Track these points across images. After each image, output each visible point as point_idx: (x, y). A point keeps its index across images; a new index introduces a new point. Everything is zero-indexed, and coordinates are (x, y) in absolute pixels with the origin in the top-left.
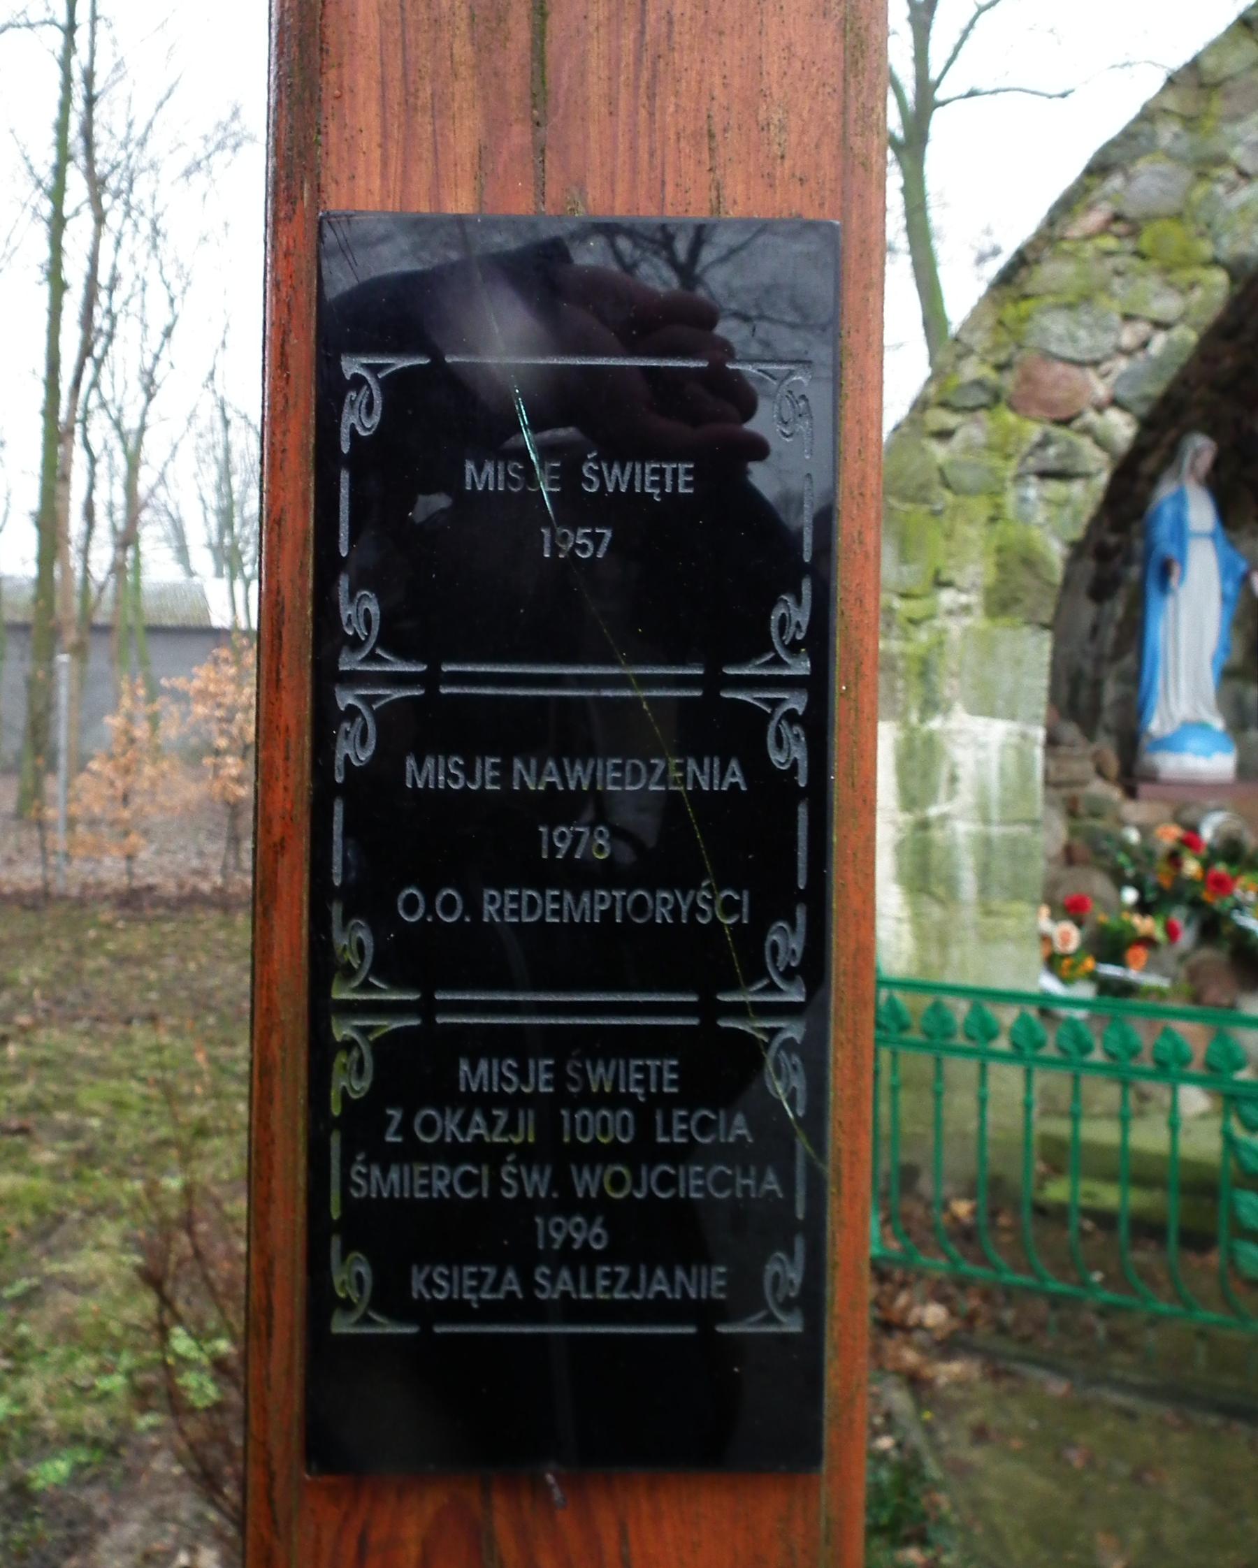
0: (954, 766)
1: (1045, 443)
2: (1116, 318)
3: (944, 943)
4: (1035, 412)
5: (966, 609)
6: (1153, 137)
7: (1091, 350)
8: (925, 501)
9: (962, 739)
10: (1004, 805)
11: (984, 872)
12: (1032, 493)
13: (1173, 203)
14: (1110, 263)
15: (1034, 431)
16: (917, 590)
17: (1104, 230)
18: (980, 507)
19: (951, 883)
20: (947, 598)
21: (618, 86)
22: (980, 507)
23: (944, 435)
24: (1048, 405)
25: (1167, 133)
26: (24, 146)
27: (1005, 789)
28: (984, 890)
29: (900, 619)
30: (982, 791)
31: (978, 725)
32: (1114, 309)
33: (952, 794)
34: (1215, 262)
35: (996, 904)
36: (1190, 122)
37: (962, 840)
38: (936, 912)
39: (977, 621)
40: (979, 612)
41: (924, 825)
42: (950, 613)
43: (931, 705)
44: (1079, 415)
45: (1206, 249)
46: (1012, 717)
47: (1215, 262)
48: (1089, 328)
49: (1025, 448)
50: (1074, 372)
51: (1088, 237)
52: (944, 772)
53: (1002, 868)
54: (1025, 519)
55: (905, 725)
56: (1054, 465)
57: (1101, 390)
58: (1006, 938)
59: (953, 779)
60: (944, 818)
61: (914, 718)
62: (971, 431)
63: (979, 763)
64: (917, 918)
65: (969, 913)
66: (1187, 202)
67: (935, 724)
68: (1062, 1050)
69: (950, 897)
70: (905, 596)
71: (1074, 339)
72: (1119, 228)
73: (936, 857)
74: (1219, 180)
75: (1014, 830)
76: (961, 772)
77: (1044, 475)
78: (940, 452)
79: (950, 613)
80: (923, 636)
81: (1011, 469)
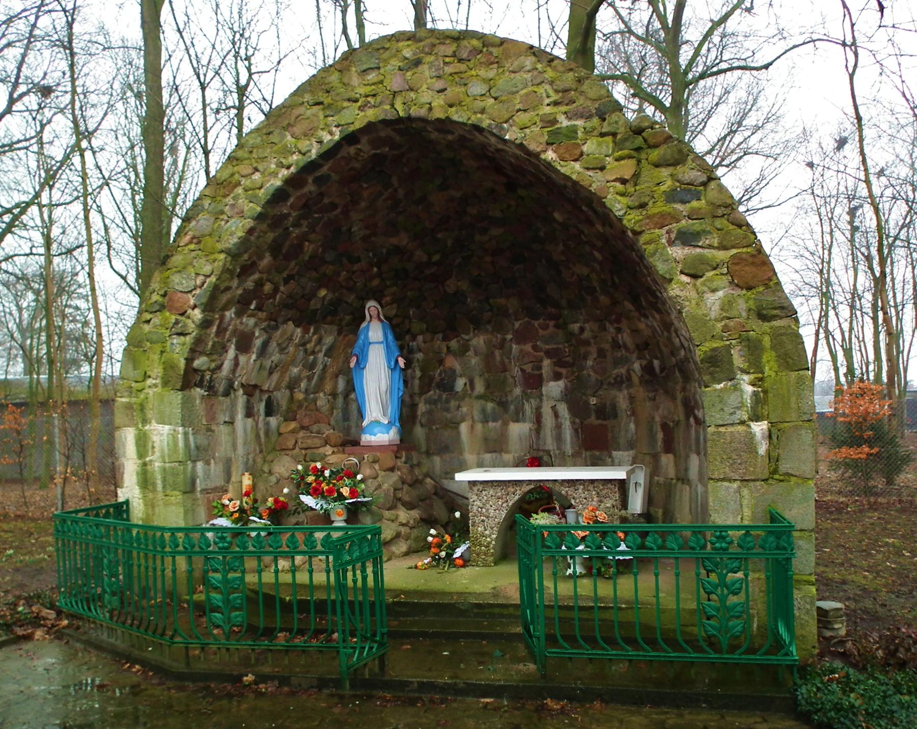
0: (153, 442)
1: (177, 322)
2: (193, 275)
3: (153, 506)
4: (174, 312)
5: (155, 385)
6: (203, 206)
7: (187, 287)
8: (142, 347)
9: (155, 433)
10: (169, 456)
11: (164, 480)
12: (175, 341)
13: (209, 230)
14: (193, 254)
15: (173, 318)
16: (140, 379)
17: (191, 242)
18: (158, 348)
19: (154, 485)
20: (149, 382)
21: (545, 175)
22: (158, 348)
23: (148, 322)
24: (177, 309)
25: (206, 203)
26: (28, 230)
27: (169, 450)
28: (164, 487)
29: (134, 390)
30: (162, 451)
31: (160, 427)
32: (192, 271)
33: (153, 453)
34: (222, 252)
35: (168, 492)
36: (213, 198)
37: (156, 469)
38: (151, 496)
39: (159, 389)
40: (160, 386)
41: (145, 464)
42: (150, 387)
43: (145, 421)
44: (186, 312)
45: (219, 246)
46: (170, 424)
47: (222, 252)
48: (186, 279)
49: (171, 325)
50: (185, 295)
51: (186, 245)
52: (150, 445)
53: (170, 480)
54: (173, 351)
55: (138, 428)
56: (179, 331)
57: (192, 302)
58: (173, 504)
59: (153, 447)
60: (151, 461)
61: (140, 426)
62: (157, 320)
63: (161, 441)
64: (144, 497)
65: (160, 496)
66: (213, 230)
67: (147, 428)
68: (185, 548)
69: (154, 490)
70: (136, 382)
71: (182, 284)
72: (195, 241)
73: (149, 476)
74: (222, 220)
75: (173, 465)
76: (155, 445)
77: (179, 334)
78: (147, 328)
79: (150, 387)
80: (142, 396)
81: (168, 333)
